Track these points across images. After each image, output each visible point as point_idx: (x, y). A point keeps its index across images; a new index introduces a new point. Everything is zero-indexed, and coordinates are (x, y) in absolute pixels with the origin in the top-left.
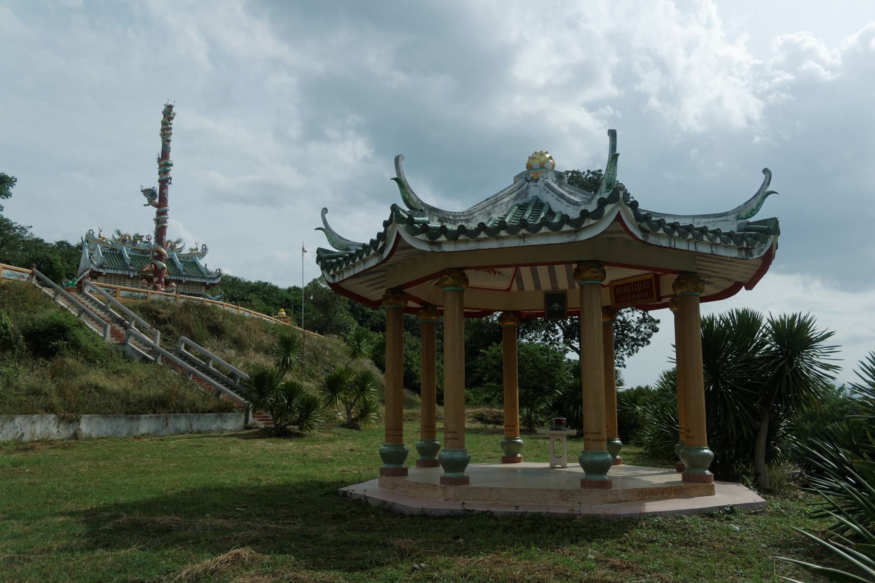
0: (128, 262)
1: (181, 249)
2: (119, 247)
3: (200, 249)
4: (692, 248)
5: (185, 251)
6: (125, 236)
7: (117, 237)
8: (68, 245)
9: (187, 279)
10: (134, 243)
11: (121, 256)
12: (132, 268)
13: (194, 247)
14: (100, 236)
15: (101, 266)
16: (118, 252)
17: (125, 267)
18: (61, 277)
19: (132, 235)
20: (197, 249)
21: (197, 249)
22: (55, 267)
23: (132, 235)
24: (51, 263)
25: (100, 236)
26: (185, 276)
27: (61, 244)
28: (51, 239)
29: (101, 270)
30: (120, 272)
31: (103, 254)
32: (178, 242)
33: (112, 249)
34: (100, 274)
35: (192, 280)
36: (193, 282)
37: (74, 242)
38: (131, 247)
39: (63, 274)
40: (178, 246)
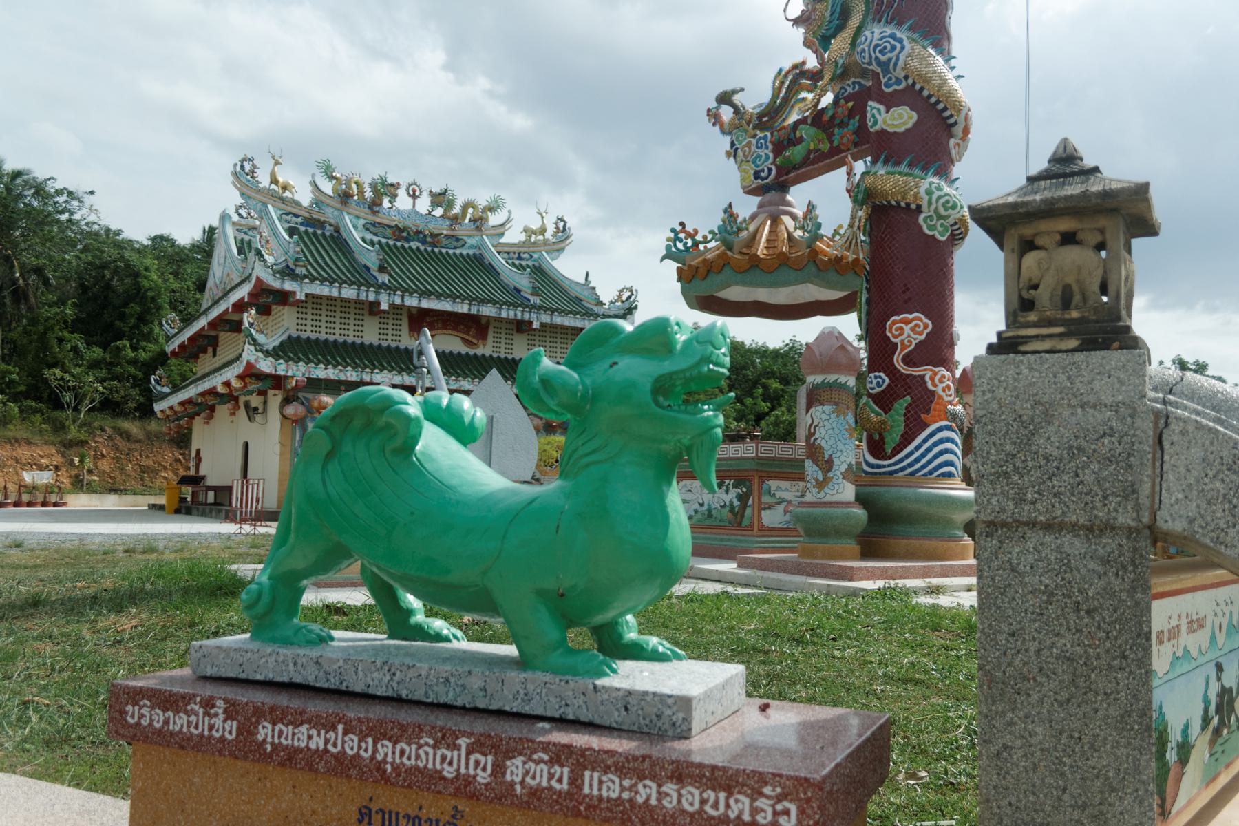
0: (371, 258)
1: (501, 229)
2: (330, 215)
3: (551, 229)
4: (335, 293)
5: (513, 236)
6: (348, 182)
7: (327, 187)
8: (172, 242)
9: (546, 318)
10: (374, 205)
11: (339, 242)
12: (384, 278)
13: (535, 226)
14: (274, 181)
15: (287, 272)
16: (329, 231)
17: (361, 276)
18: (159, 308)
19: (366, 181)
20: (543, 231)
21: (543, 231)
22: (145, 283)
23: (366, 181)
24: (136, 275)
25: (274, 181)
26: (539, 309)
27: (159, 240)
28: (138, 231)
29: (289, 286)
30: (349, 293)
31: (292, 231)
32: (491, 209)
33: (310, 222)
34: (284, 298)
35: (558, 320)
36: (564, 328)
37: (186, 235)
38: (366, 216)
39: (164, 300)
40: (494, 219)
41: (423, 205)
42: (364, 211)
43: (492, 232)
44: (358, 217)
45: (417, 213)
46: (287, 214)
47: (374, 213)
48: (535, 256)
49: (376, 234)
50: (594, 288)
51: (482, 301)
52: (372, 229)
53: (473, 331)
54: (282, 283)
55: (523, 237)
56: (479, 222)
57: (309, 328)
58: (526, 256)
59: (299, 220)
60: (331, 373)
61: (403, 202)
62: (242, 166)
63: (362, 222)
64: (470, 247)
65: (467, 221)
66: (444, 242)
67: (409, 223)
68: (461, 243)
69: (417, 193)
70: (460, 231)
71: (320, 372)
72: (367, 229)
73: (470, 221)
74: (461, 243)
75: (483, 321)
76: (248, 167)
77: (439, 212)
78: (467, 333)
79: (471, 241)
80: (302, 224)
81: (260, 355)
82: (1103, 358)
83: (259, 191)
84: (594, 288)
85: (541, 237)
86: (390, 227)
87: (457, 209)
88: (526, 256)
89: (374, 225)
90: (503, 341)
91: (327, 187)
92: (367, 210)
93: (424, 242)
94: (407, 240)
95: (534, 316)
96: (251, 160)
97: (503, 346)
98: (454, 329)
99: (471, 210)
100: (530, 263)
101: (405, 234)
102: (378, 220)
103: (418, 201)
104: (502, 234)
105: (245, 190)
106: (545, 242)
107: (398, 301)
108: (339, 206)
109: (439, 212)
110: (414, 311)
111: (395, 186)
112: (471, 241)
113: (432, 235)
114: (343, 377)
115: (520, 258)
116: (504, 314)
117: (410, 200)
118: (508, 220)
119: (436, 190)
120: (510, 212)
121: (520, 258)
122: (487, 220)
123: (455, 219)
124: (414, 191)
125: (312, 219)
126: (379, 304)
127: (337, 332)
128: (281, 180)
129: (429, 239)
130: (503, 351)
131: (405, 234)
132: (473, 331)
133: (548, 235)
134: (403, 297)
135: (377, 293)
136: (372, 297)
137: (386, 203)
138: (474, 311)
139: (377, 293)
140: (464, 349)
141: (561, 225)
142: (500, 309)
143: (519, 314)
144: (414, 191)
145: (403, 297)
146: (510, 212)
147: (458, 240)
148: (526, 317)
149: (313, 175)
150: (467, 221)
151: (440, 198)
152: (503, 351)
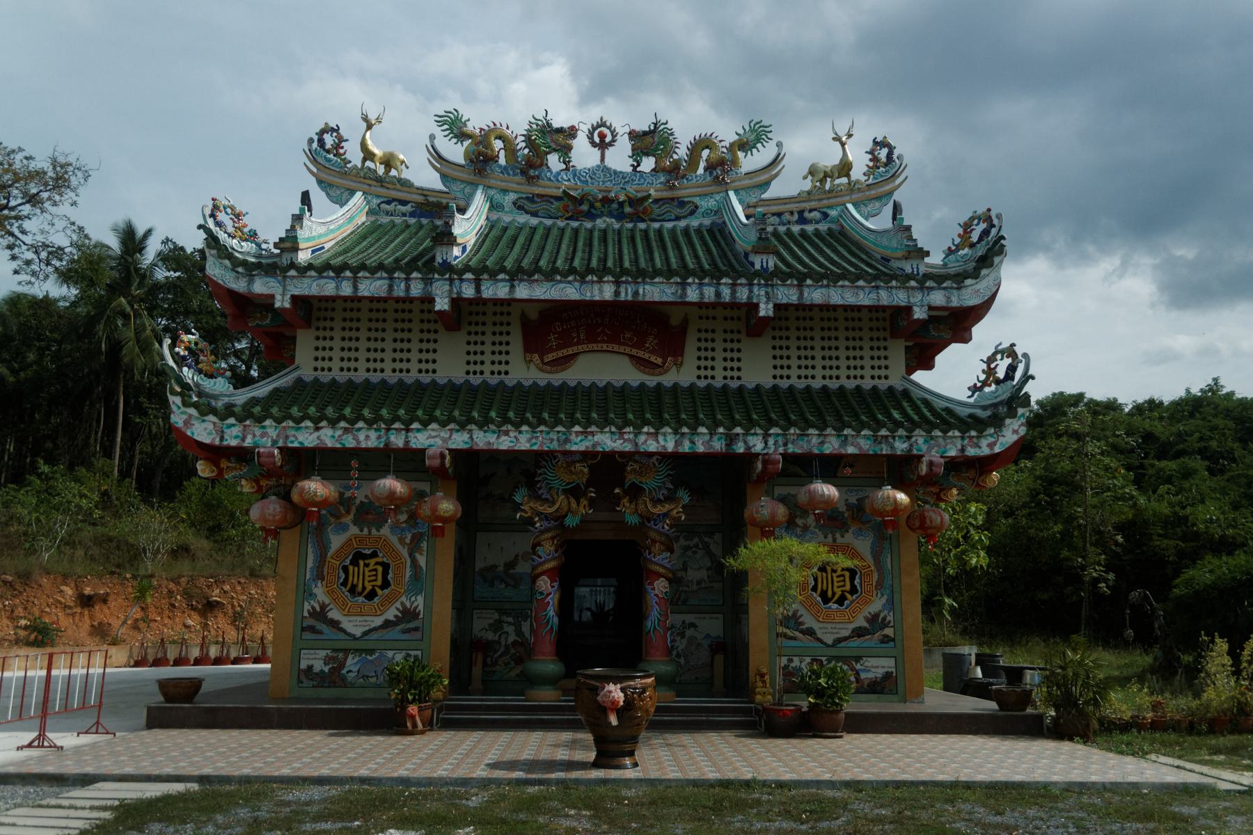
4: (346, 290)
5: (789, 184)
9: (786, 294)
10: (530, 167)
21: (845, 167)
25: (368, 155)
32: (744, 145)
35: (816, 295)
41: (620, 158)
42: (516, 182)
43: (747, 182)
44: (505, 191)
45: (606, 170)
46: (388, 203)
47: (531, 180)
48: (833, 213)
49: (535, 214)
50: (908, 228)
51: (641, 275)
52: (528, 206)
53: (651, 342)
54: (251, 282)
55: (807, 185)
56: (721, 168)
57: (336, 364)
58: (816, 215)
59: (408, 208)
60: (328, 437)
61: (584, 155)
62: (321, 142)
63: (512, 197)
64: (706, 214)
65: (701, 171)
66: (657, 210)
67: (593, 189)
68: (688, 208)
69: (608, 139)
70: (685, 190)
71: (306, 437)
72: (520, 208)
73: (706, 169)
74: (688, 208)
75: (675, 320)
76: (329, 140)
77: (648, 164)
78: (640, 345)
79: (706, 204)
80: (412, 215)
81: (192, 411)
82: (921, 771)
83: (344, 174)
84: (908, 228)
85: (844, 180)
86: (558, 199)
87: (682, 152)
88: (816, 215)
89: (531, 199)
90: (719, 355)
91: (456, 152)
92: (519, 178)
93: (620, 217)
94: (591, 216)
95: (759, 293)
96: (337, 130)
97: (719, 364)
98: (613, 339)
99: (705, 153)
100: (823, 227)
101: (585, 207)
102: (537, 190)
103: (608, 153)
104: (766, 185)
105: (323, 176)
106: (852, 187)
107: (468, 291)
108: (471, 177)
109: (648, 164)
110: (533, 315)
111: (572, 132)
112: (706, 204)
113: (632, 202)
114: (350, 442)
115: (802, 220)
116: (692, 295)
117: (596, 152)
118: (775, 162)
119: (643, 125)
120: (779, 145)
121: (802, 220)
122: (735, 162)
123: (674, 171)
124: (602, 136)
125: (428, 203)
126: (432, 301)
127: (388, 366)
128: (378, 152)
129: (628, 209)
130: (719, 373)
131: (585, 207)
132: (651, 342)
133: (858, 173)
134: (478, 283)
135: (427, 281)
136: (416, 290)
137: (554, 161)
138: (626, 294)
139: (427, 281)
140: (632, 376)
141: (883, 154)
142: (684, 285)
143: (726, 293)
144: (602, 136)
145: (478, 283)
146: (779, 145)
147: (682, 204)
148: (743, 295)
149: (432, 137)
150: (701, 171)
151: (650, 141)
152: (719, 373)
